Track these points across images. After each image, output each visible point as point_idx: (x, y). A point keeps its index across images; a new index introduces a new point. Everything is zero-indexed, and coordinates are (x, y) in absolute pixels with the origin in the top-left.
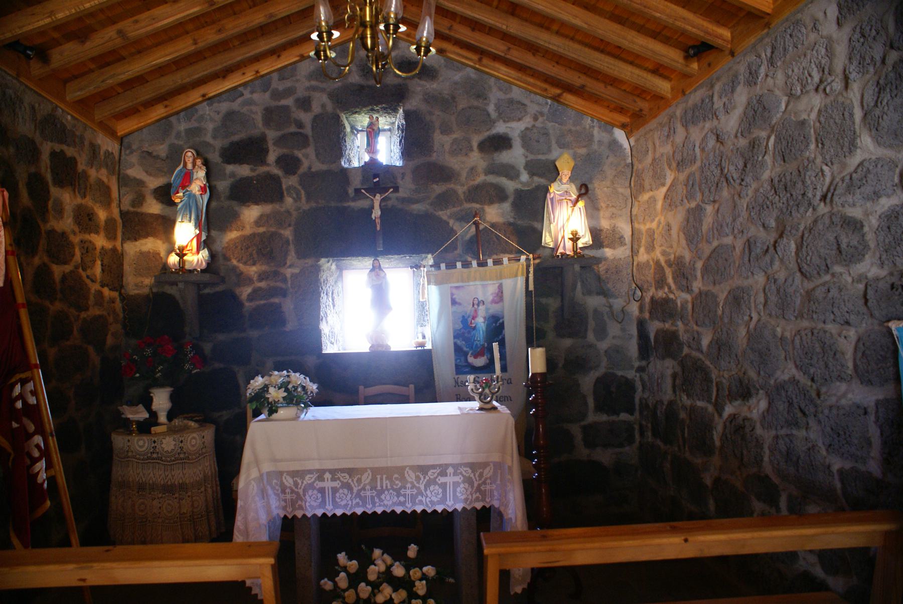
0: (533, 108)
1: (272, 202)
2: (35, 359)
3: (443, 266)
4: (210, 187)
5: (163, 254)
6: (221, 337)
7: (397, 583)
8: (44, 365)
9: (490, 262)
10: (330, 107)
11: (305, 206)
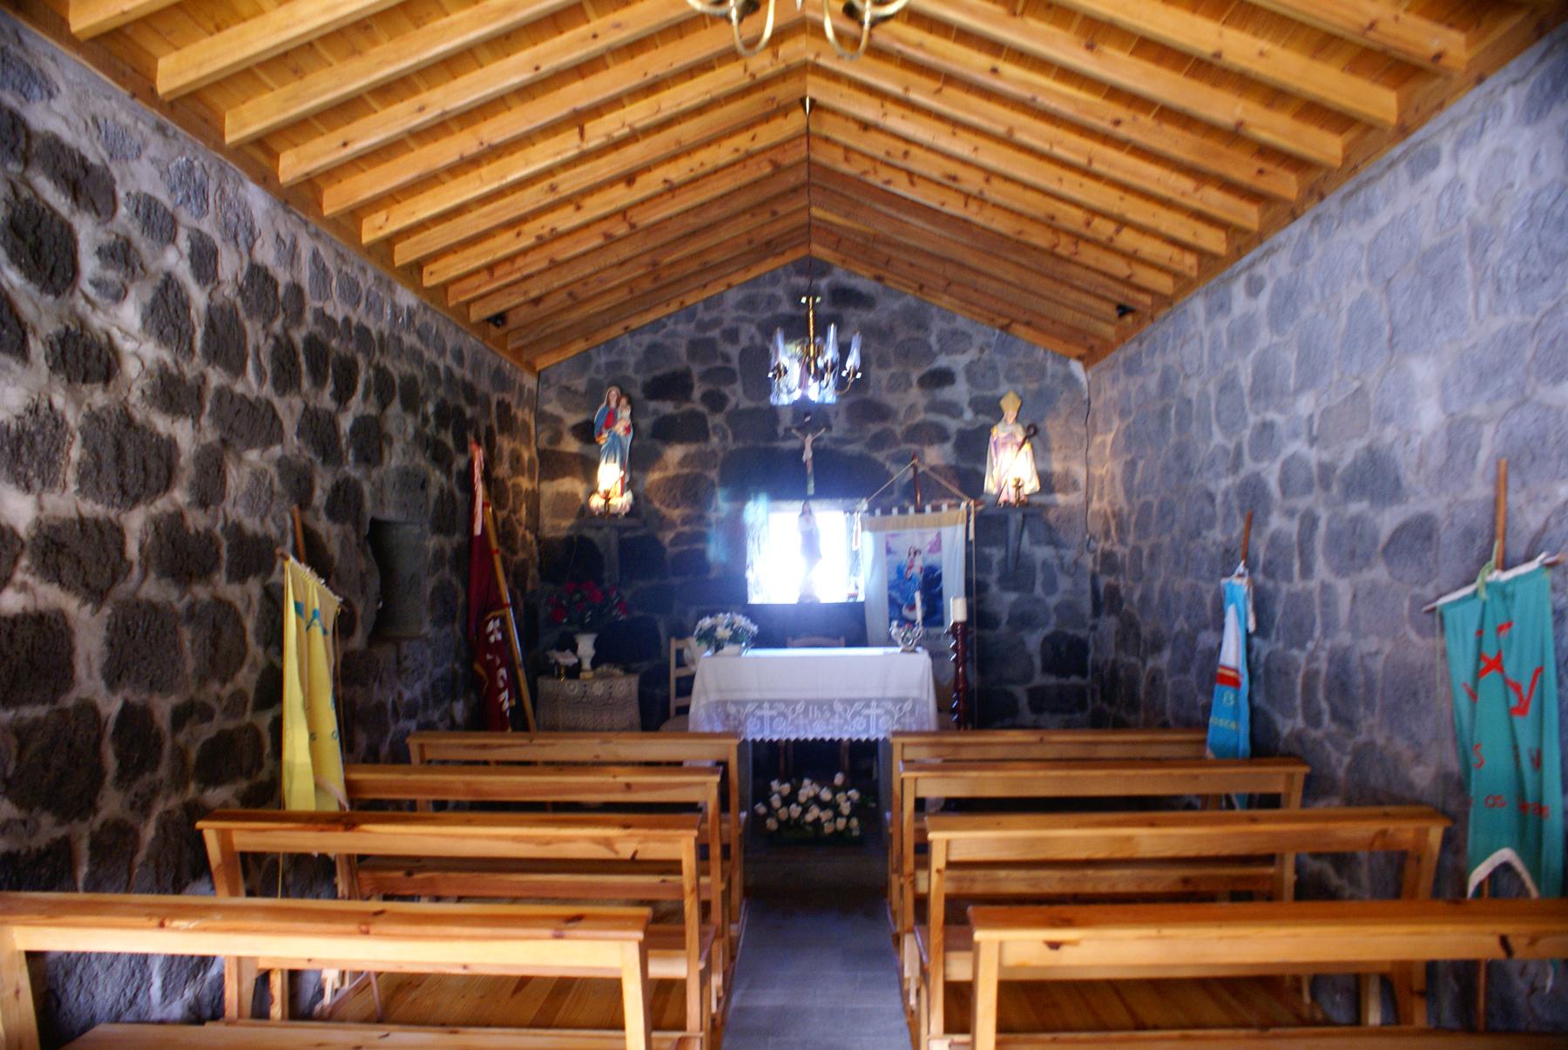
0: (978, 340)
1: (697, 440)
2: (507, 599)
3: (878, 512)
4: (634, 427)
5: (581, 495)
6: (641, 584)
7: (823, 805)
8: (514, 604)
9: (928, 508)
10: (758, 340)
11: (731, 445)
